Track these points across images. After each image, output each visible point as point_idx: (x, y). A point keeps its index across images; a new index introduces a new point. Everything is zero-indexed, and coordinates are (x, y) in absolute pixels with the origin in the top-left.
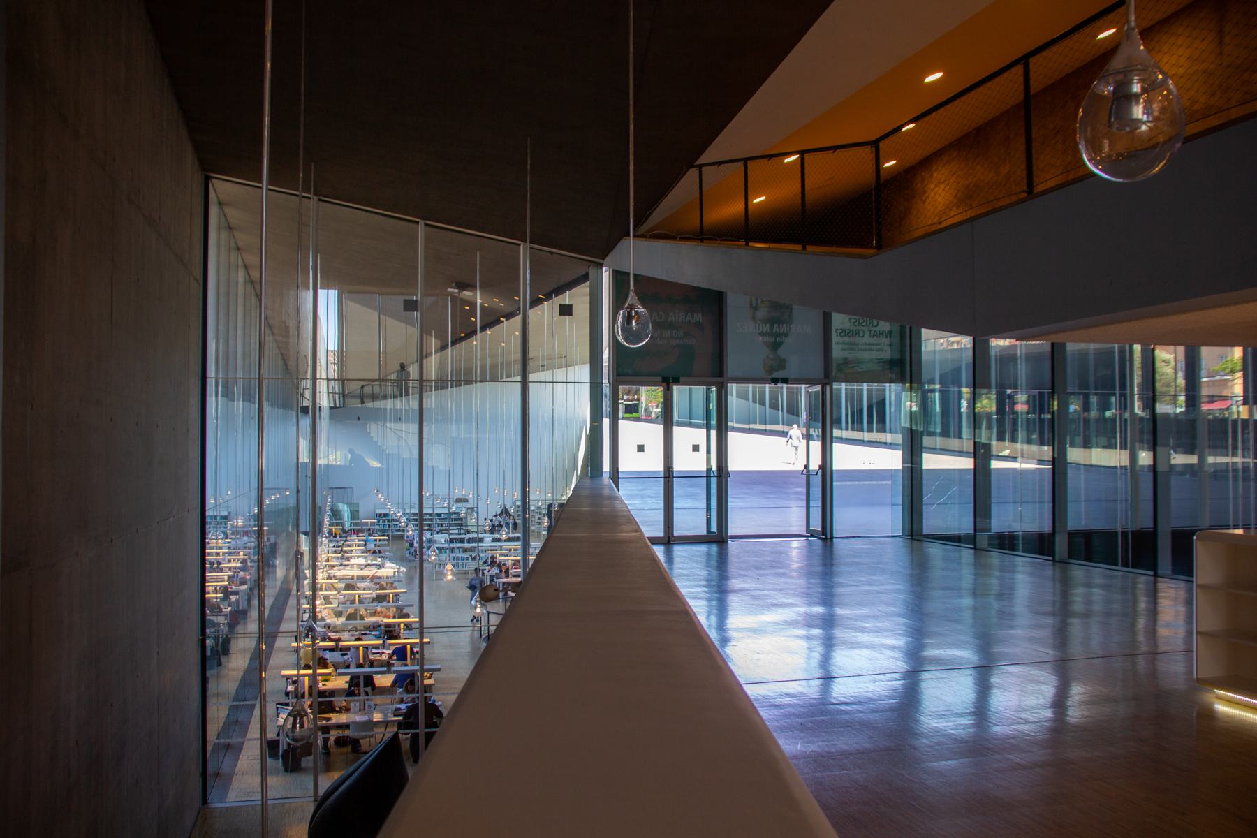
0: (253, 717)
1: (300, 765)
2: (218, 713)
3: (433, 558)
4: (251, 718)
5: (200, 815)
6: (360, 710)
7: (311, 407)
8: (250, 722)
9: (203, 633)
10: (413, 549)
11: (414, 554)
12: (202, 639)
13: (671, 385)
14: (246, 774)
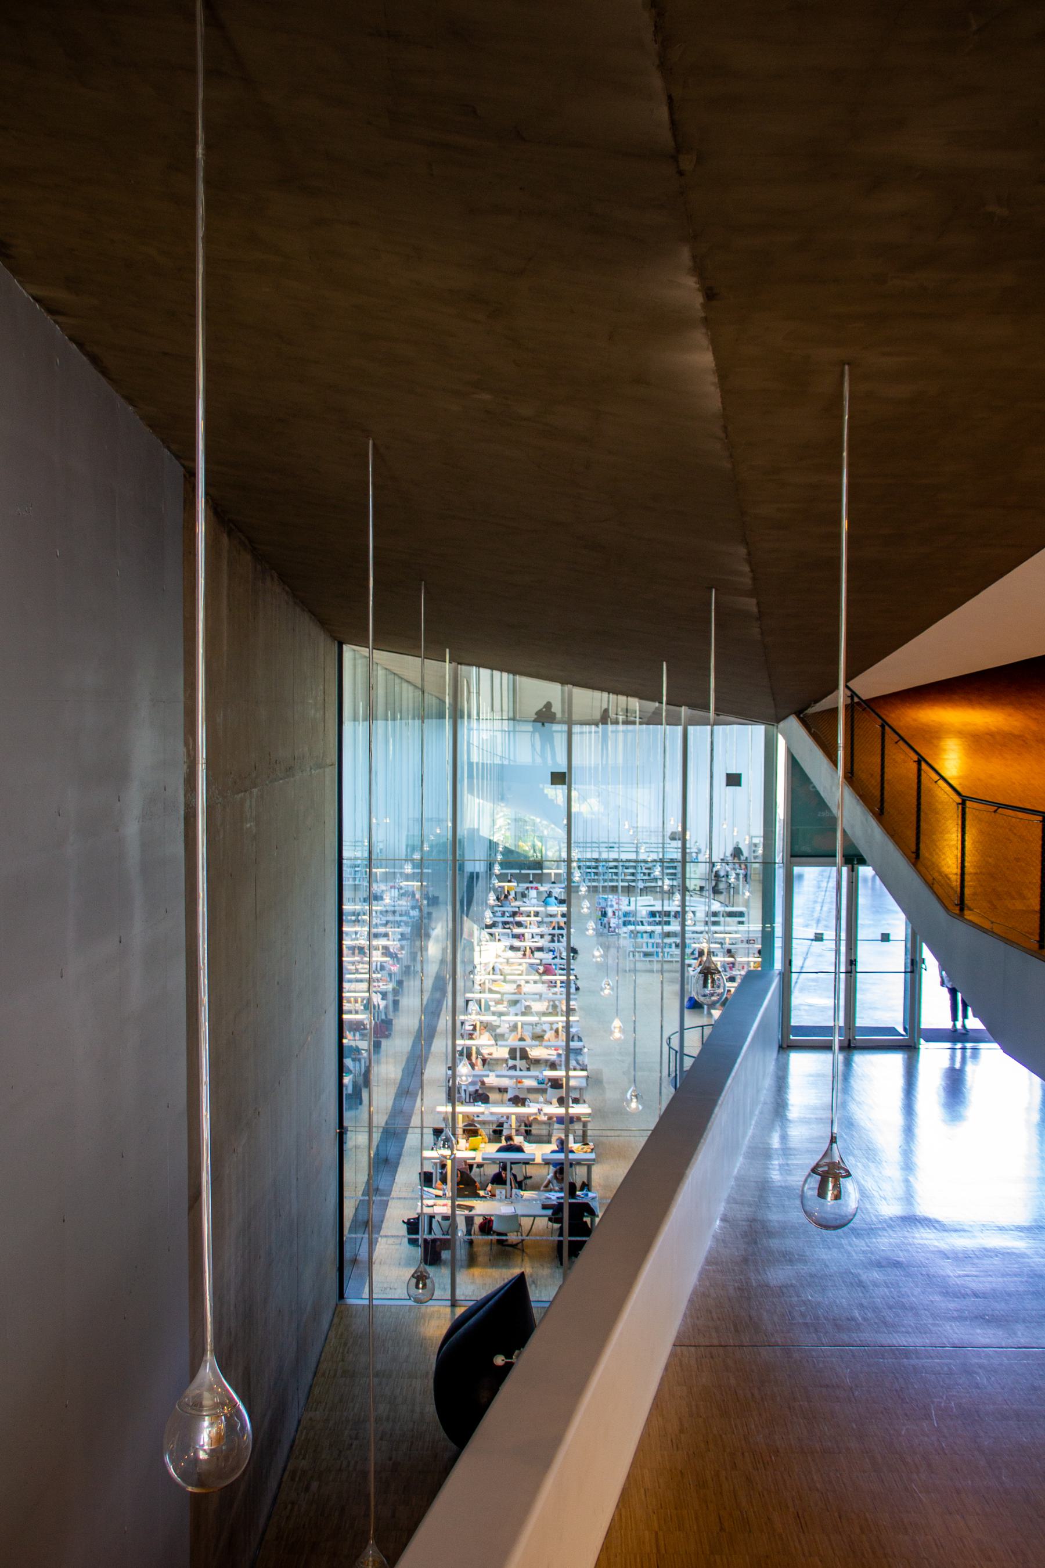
0: (395, 1184)
1: (441, 1257)
2: (356, 1175)
3: (607, 992)
4: (392, 1186)
5: (336, 1313)
6: (506, 1197)
7: (466, 792)
8: (391, 1191)
9: (341, 1070)
10: (606, 919)
11: (607, 926)
12: (339, 1132)
13: (855, 866)
14: (385, 1263)
